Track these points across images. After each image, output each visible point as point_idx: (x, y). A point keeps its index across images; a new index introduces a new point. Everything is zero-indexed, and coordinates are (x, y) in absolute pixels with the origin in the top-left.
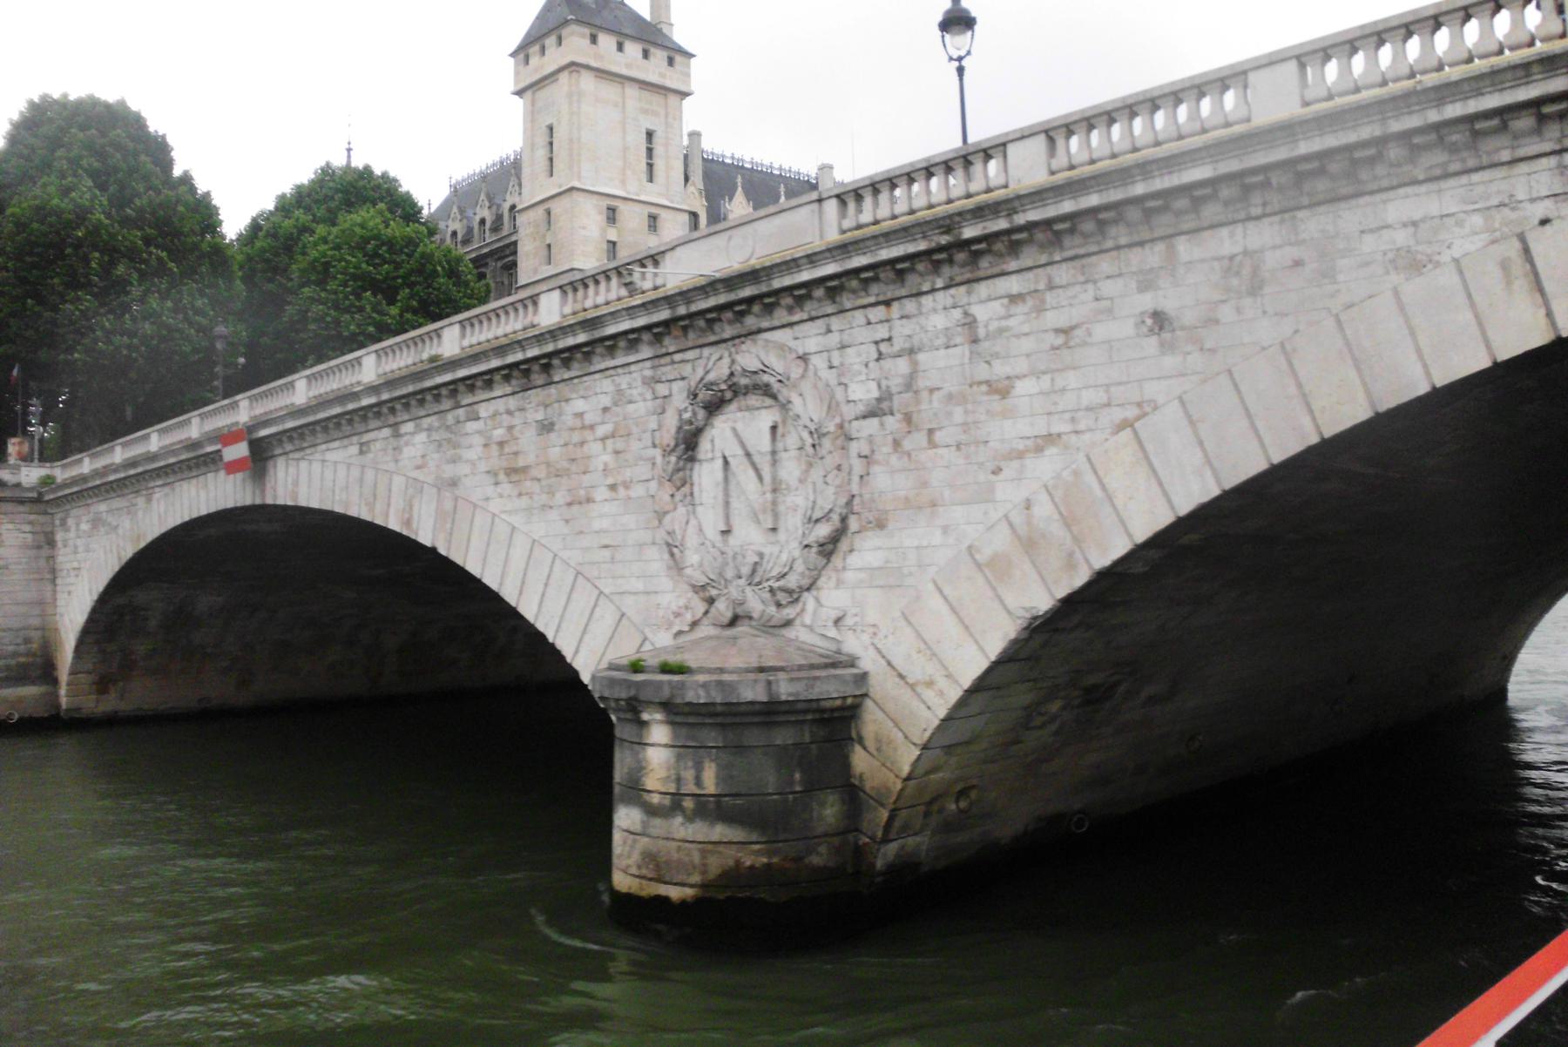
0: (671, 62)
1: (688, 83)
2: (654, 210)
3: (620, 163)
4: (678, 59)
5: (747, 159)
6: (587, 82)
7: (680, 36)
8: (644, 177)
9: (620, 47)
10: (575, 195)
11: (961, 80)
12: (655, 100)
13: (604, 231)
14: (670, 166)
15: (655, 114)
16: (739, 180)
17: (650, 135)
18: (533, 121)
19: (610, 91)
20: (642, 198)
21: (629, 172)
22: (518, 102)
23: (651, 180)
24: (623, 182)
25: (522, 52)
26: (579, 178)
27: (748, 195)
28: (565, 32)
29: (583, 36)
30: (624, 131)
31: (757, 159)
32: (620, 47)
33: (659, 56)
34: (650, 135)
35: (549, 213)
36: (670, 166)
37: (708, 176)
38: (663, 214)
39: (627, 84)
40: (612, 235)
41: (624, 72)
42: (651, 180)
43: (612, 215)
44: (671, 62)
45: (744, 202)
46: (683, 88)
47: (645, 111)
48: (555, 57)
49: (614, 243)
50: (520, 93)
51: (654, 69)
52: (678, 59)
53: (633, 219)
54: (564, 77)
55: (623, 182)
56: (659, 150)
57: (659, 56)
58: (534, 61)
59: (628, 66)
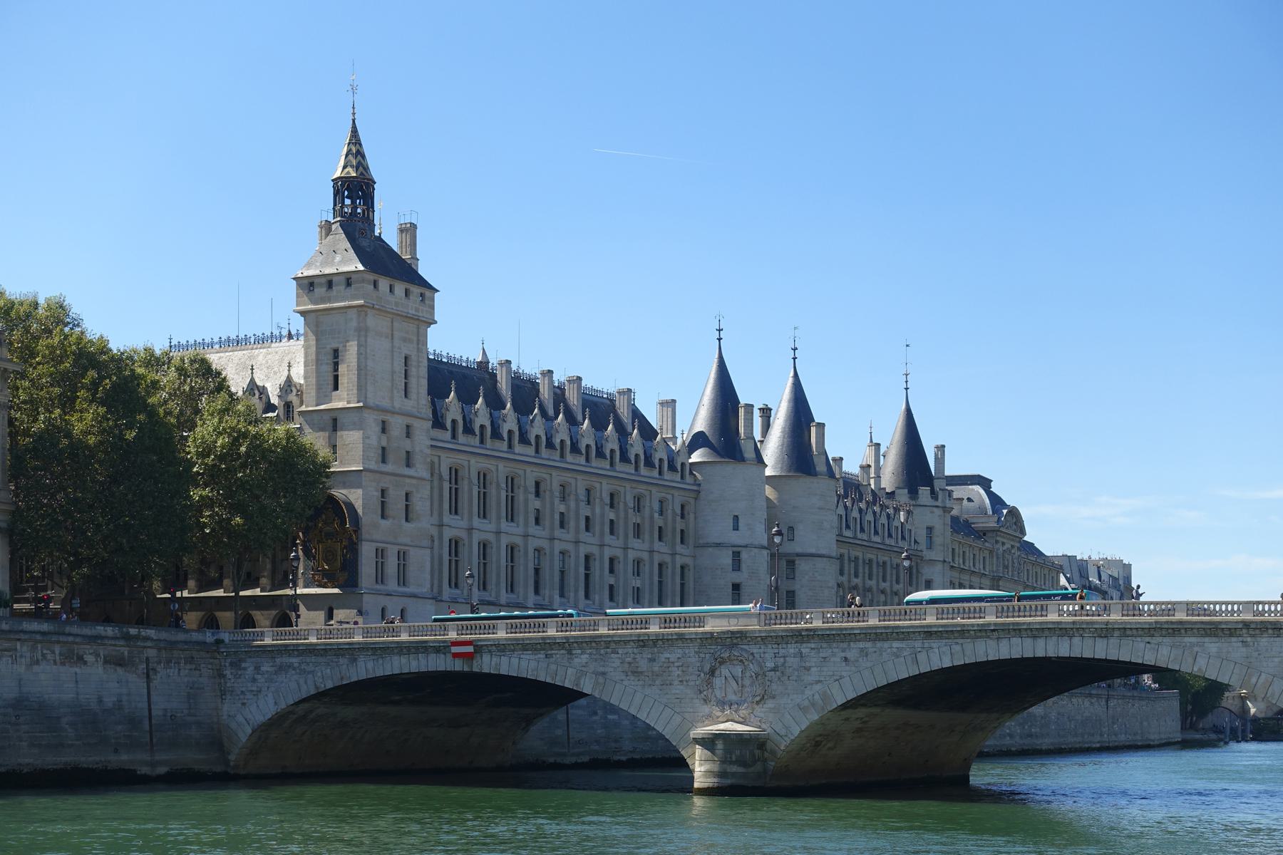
1: (433, 314)
7: (423, 271)
13: (380, 438)
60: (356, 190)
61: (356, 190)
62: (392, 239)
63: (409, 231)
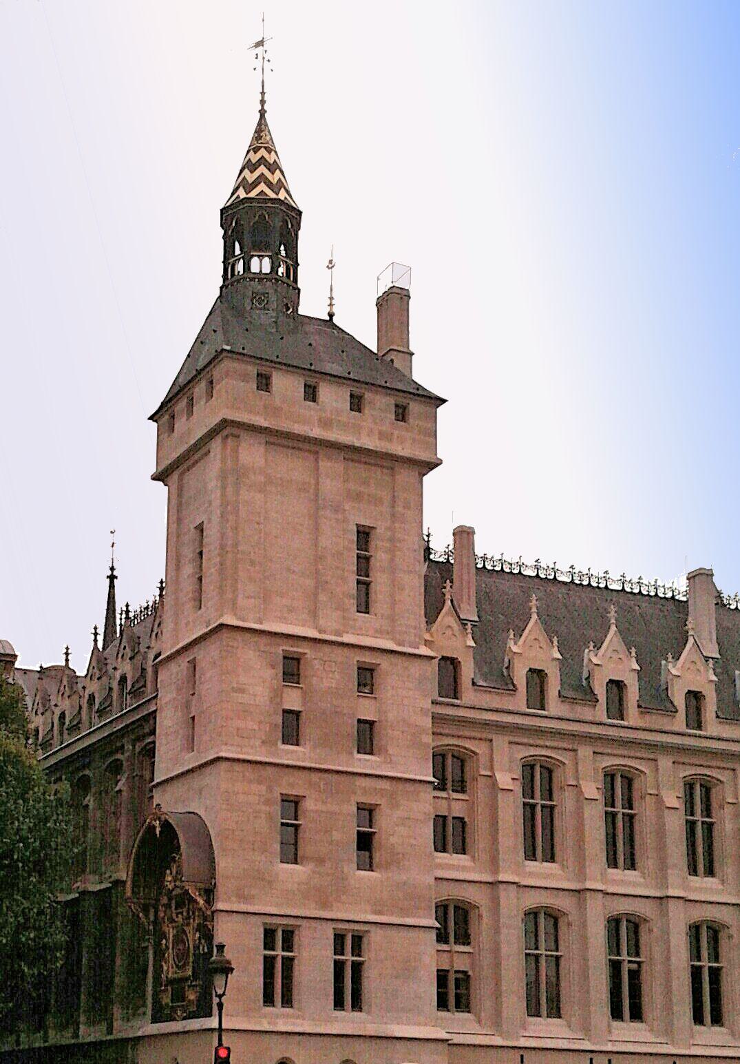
0: (401, 414)
2: (368, 658)
3: (310, 583)
4: (415, 407)
5: (563, 566)
6: (252, 453)
8: (352, 604)
9: (311, 394)
10: (225, 634)
11: (262, 113)
12: (375, 480)
13: (277, 695)
14: (401, 588)
15: (378, 501)
16: (612, 615)
17: (364, 535)
18: (179, 520)
19: (292, 467)
20: (348, 638)
21: (322, 597)
22: (161, 489)
23: (365, 606)
24: (314, 614)
25: (164, 415)
26: (234, 610)
27: (626, 636)
28: (217, 372)
29: (244, 377)
30: (316, 528)
31: (581, 567)
32: (311, 394)
33: (380, 406)
34: (364, 535)
35: (193, 664)
36: (401, 588)
37: (484, 599)
38: (384, 663)
39: (322, 452)
40: (293, 700)
41: (317, 432)
42: (365, 606)
43: (292, 670)
44: (401, 414)
45: (543, 637)
46: (424, 456)
47: (358, 497)
48: (205, 416)
49: (371, 724)
50: (159, 477)
51: (372, 430)
52: (415, 407)
53: (329, 677)
54: (216, 445)
55: (314, 614)
56: (379, 557)
57: (380, 406)
58: (180, 424)
59: (326, 423)
60: (260, 224)
61: (260, 224)
62: (363, 327)
63: (394, 305)
